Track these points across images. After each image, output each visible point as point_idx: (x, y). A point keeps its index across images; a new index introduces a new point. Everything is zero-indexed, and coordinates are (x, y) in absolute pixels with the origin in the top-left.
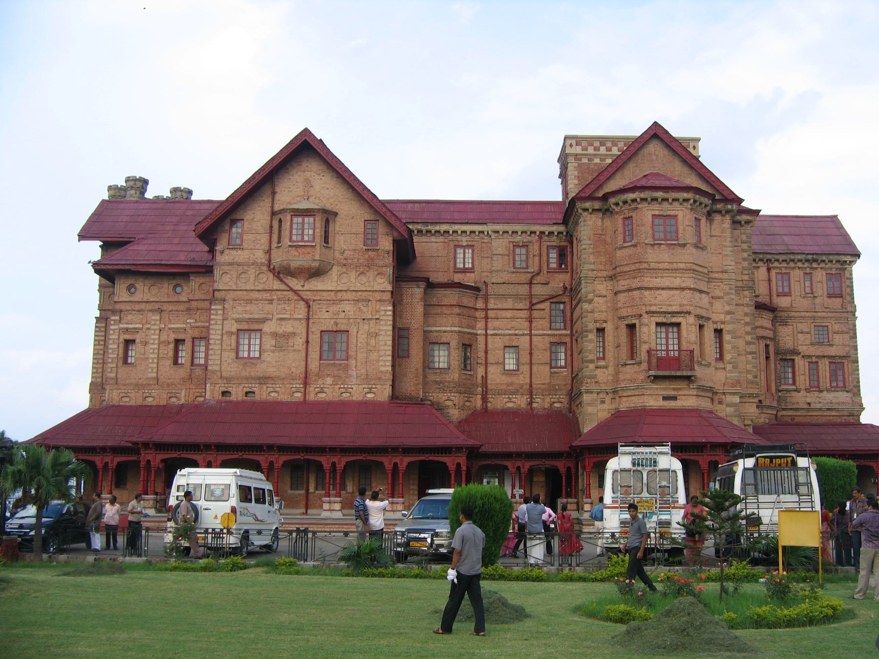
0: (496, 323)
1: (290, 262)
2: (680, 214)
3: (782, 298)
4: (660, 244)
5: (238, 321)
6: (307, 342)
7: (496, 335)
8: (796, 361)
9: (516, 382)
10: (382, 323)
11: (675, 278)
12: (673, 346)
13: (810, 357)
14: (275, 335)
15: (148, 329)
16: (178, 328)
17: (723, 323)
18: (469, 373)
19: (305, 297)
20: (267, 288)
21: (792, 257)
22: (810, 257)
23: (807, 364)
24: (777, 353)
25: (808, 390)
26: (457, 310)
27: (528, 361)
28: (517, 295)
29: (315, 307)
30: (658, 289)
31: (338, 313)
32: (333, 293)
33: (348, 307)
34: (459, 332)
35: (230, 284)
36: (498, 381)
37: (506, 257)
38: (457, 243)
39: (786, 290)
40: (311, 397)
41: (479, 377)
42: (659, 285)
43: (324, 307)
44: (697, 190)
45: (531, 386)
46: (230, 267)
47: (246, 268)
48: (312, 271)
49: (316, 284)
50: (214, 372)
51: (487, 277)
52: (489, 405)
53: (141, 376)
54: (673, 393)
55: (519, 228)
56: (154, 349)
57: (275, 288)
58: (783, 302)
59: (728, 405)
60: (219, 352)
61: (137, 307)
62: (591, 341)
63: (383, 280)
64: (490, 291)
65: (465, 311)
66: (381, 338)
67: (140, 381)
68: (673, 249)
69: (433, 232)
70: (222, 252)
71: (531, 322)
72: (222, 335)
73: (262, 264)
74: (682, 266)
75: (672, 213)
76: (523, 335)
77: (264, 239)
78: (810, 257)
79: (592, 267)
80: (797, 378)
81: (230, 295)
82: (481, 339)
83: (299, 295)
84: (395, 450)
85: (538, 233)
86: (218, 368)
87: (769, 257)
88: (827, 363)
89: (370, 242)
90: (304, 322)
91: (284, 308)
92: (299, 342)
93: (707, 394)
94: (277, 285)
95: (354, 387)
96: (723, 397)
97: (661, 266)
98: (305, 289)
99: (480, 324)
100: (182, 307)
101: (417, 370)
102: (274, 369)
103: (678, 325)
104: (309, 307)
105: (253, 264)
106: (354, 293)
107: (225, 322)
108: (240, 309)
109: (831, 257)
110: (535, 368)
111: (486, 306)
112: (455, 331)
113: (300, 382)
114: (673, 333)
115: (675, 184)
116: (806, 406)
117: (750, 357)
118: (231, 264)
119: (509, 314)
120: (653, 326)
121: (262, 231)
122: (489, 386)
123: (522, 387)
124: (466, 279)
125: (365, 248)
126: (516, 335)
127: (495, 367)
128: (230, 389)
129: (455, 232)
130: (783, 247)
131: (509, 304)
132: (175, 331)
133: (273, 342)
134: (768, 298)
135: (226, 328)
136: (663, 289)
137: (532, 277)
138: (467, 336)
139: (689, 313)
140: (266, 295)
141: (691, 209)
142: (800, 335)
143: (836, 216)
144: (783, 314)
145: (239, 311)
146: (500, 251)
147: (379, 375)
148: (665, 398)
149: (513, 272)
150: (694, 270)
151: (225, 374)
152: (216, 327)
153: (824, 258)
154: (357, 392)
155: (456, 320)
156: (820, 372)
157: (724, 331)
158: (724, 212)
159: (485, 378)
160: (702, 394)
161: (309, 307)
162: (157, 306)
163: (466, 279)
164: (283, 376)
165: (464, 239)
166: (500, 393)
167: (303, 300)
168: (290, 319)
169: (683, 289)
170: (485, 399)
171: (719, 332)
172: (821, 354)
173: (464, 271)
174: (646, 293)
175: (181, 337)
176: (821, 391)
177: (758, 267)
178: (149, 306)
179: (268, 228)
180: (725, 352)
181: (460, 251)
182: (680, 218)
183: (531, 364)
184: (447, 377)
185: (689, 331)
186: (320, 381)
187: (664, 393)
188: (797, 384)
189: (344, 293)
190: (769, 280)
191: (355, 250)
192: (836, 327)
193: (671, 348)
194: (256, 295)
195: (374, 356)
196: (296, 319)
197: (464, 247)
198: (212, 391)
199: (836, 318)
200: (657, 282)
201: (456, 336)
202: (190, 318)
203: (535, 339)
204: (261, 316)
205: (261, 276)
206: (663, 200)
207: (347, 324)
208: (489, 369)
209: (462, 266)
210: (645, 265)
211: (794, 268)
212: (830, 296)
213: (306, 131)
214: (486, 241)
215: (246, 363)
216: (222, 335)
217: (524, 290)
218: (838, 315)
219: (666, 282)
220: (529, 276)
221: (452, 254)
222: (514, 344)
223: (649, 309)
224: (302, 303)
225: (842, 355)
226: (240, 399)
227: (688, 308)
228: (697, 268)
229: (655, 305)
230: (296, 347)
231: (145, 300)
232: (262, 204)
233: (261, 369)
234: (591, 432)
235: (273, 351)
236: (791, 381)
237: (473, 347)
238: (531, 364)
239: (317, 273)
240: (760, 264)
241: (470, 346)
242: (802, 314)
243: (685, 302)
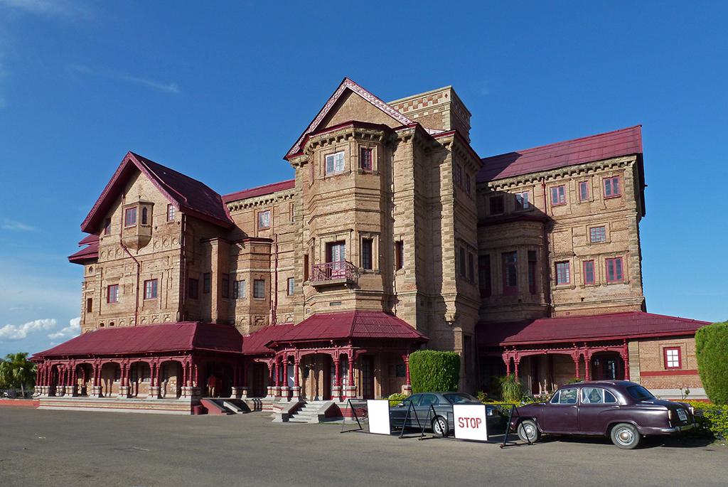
3: (557, 209)
7: (283, 271)
10: (174, 271)
11: (342, 202)
22: (583, 166)
23: (582, 263)
25: (583, 287)
27: (286, 288)
31: (151, 269)
33: (158, 263)
37: (288, 214)
42: (329, 212)
49: (144, 251)
51: (277, 230)
58: (557, 212)
65: (258, 257)
68: (340, 179)
79: (301, 208)
81: (106, 264)
88: (604, 260)
94: (126, 255)
97: (329, 195)
99: (273, 265)
104: (139, 266)
118: (105, 246)
127: (281, 293)
130: (576, 161)
136: (331, 214)
140: (121, 262)
145: (109, 274)
146: (284, 211)
166: (283, 311)
169: (346, 211)
174: (318, 220)
187: (329, 299)
194: (116, 263)
200: (328, 209)
201: (248, 274)
210: (318, 197)
219: (335, 208)
229: (325, 228)
235: (123, 296)
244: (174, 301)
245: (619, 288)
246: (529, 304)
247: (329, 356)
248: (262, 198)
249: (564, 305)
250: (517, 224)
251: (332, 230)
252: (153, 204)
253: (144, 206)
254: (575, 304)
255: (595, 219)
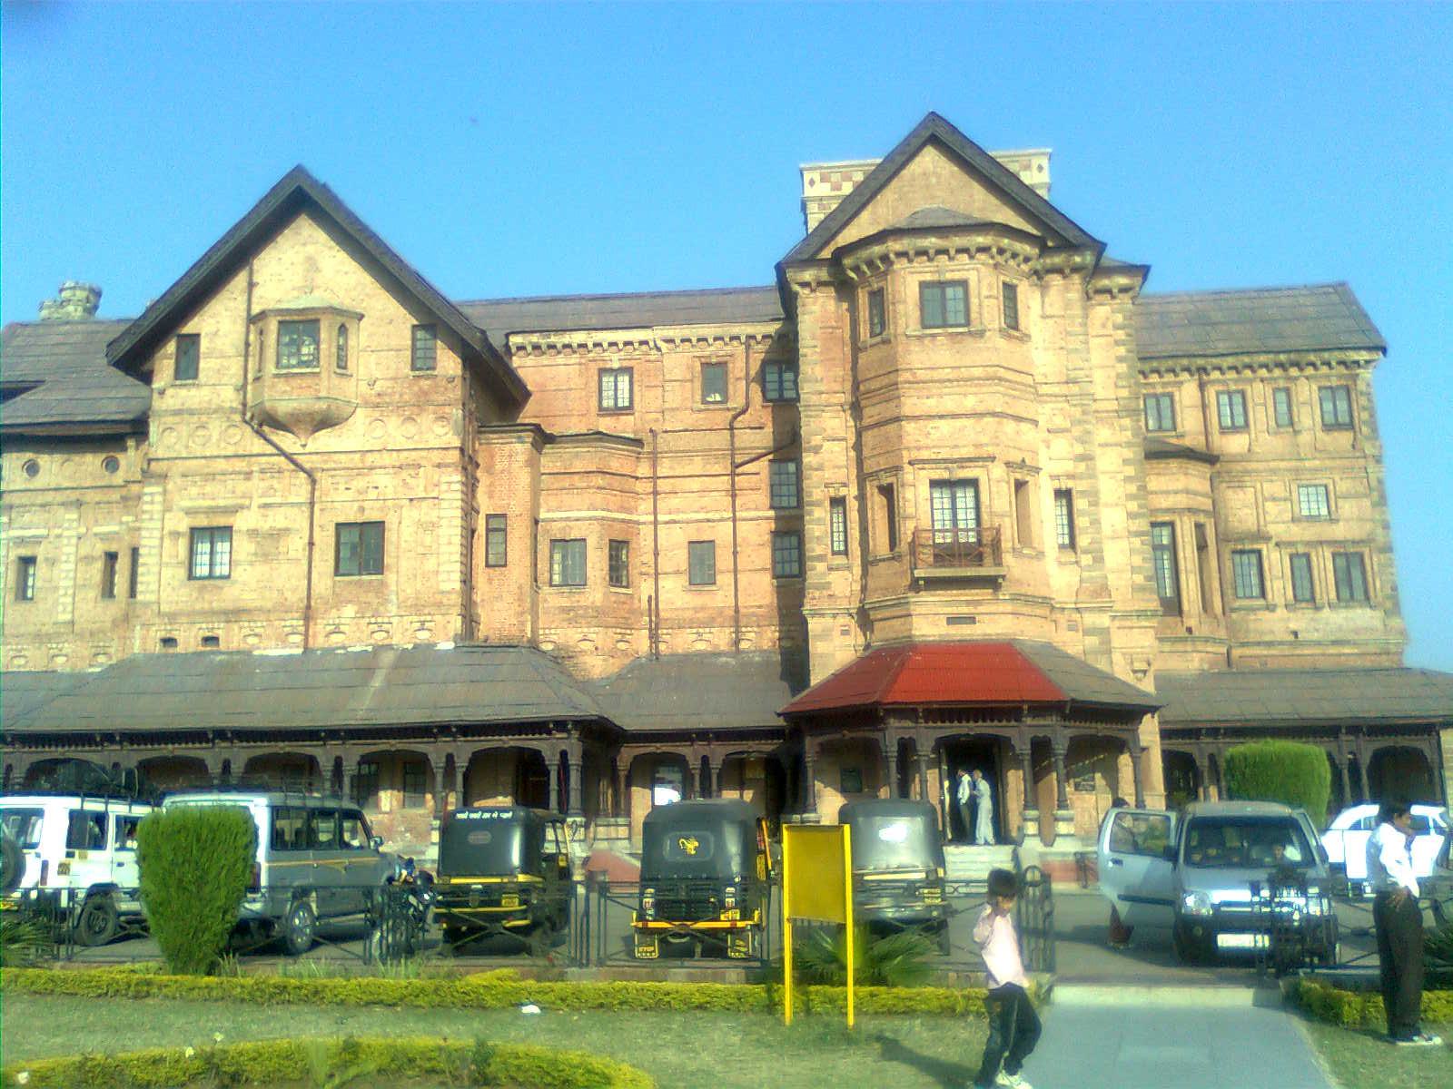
0: (675, 502)
1: (277, 404)
2: (972, 277)
4: (934, 336)
5: (189, 512)
6: (311, 544)
7: (744, 520)
8: (1265, 553)
9: (710, 604)
12: (966, 517)
13: (1291, 544)
14: (253, 533)
15: (59, 536)
16: (109, 533)
17: (1071, 476)
18: (624, 590)
19: (307, 466)
20: (241, 452)
21: (1247, 360)
22: (1282, 357)
24: (1222, 538)
26: (600, 481)
27: (732, 567)
28: (710, 450)
29: (324, 481)
30: (931, 417)
32: (357, 456)
33: (384, 480)
34: (603, 519)
35: (177, 447)
36: (679, 604)
37: (688, 384)
38: (602, 365)
39: (1240, 421)
40: (319, 641)
41: (645, 598)
43: (342, 480)
44: (1006, 230)
45: (737, 611)
46: (177, 419)
47: (204, 418)
48: (318, 418)
49: (325, 440)
50: (146, 605)
51: (657, 420)
52: (662, 647)
53: (46, 620)
54: (965, 610)
55: (709, 331)
56: (68, 571)
57: (255, 451)
58: (1235, 444)
59: (1087, 632)
60: (155, 569)
61: (40, 499)
62: (819, 521)
63: (446, 429)
64: (662, 446)
65: (616, 482)
66: (441, 531)
67: (44, 629)
68: (960, 342)
69: (559, 346)
70: (162, 392)
71: (734, 496)
72: (162, 539)
73: (233, 410)
74: (977, 372)
75: (957, 276)
76: (722, 520)
77: (235, 366)
78: (1282, 357)
80: (1268, 584)
81: (180, 466)
82: (646, 531)
83: (293, 461)
84: (444, 729)
85: (743, 339)
86: (153, 598)
87: (1200, 362)
88: (1328, 555)
89: (421, 362)
90: (306, 509)
91: (272, 487)
92: (297, 545)
93: (1039, 611)
94: (258, 445)
95: (395, 620)
96: (1076, 616)
98: (307, 450)
100: (116, 496)
101: (520, 587)
102: (254, 596)
103: (974, 483)
104: (314, 482)
105: (215, 411)
106: (395, 454)
107: (168, 515)
108: (194, 491)
109: (1326, 355)
110: (742, 578)
111: (655, 472)
112: (596, 519)
113: (297, 615)
114: (965, 498)
115: (961, 221)
116: (1292, 638)
117: (1137, 542)
118: (178, 412)
119: (695, 484)
120: (924, 489)
121: (232, 352)
122: (662, 614)
123: (721, 611)
124: (620, 428)
125: (412, 373)
126: (708, 521)
128: (175, 634)
129: (597, 345)
131: (697, 466)
132: (104, 537)
133: (252, 547)
134: (1202, 439)
135: (169, 526)
136: (941, 417)
137: (735, 417)
138: (617, 526)
139: (993, 459)
140: (240, 465)
141: (996, 266)
142: (1269, 505)
143: (1343, 284)
144: (1239, 467)
147: (439, 597)
148: (953, 620)
149: (700, 411)
150: (1000, 379)
151: (165, 608)
152: (150, 525)
153: (1312, 357)
154: (404, 633)
155: (599, 498)
156: (1315, 573)
157: (1074, 493)
158: (1067, 271)
159: (654, 600)
160: (1025, 610)
161: (314, 482)
162: (73, 496)
163: (620, 428)
164: (269, 605)
165: (615, 357)
167: (303, 470)
168: (280, 505)
170: (654, 637)
171: (1064, 495)
172: (1314, 538)
173: (617, 411)
175: (113, 548)
176: (1317, 609)
177: (1182, 383)
178: (60, 497)
179: (242, 346)
180: (1077, 532)
181: (608, 380)
182: (973, 285)
183: (735, 571)
184: (582, 598)
185: (998, 497)
186: (334, 613)
187: (949, 610)
188: (1270, 596)
189: (377, 455)
190: (1204, 407)
191: (394, 379)
192: (1343, 486)
193: (961, 525)
194: (221, 465)
195: (431, 564)
196: (292, 504)
197: (616, 372)
198: (144, 639)
199: (1343, 470)
200: (931, 405)
202: (128, 514)
203: (741, 526)
204: (229, 502)
205: (232, 431)
206: (940, 252)
207: (382, 509)
208: (661, 583)
209: (611, 403)
211: (1250, 381)
212: (1327, 428)
213: (299, 171)
214: (652, 358)
215: (204, 587)
216: (162, 539)
217: (721, 439)
218: (1346, 462)
219: (949, 404)
220: (730, 415)
221: (594, 385)
222: (705, 538)
223: (915, 455)
224: (302, 475)
225: (1357, 538)
226: (191, 650)
227: (990, 450)
228: (1009, 375)
229: (927, 448)
230: (292, 554)
231: (53, 486)
232: (232, 304)
233: (230, 595)
234: (825, 685)
235: (251, 564)
236: (1256, 591)
237: (633, 545)
238: (735, 571)
239: (324, 422)
240: (1185, 376)
241: (627, 542)
242: (1272, 465)
243: (984, 440)
244: (446, 587)
245: (1361, 618)
246: (1207, 640)
247: (536, 756)
248: (621, 336)
249: (1258, 644)
250: (1174, 464)
251: (945, 454)
252: (361, 317)
253: (340, 320)
254: (1281, 643)
255: (1310, 470)
